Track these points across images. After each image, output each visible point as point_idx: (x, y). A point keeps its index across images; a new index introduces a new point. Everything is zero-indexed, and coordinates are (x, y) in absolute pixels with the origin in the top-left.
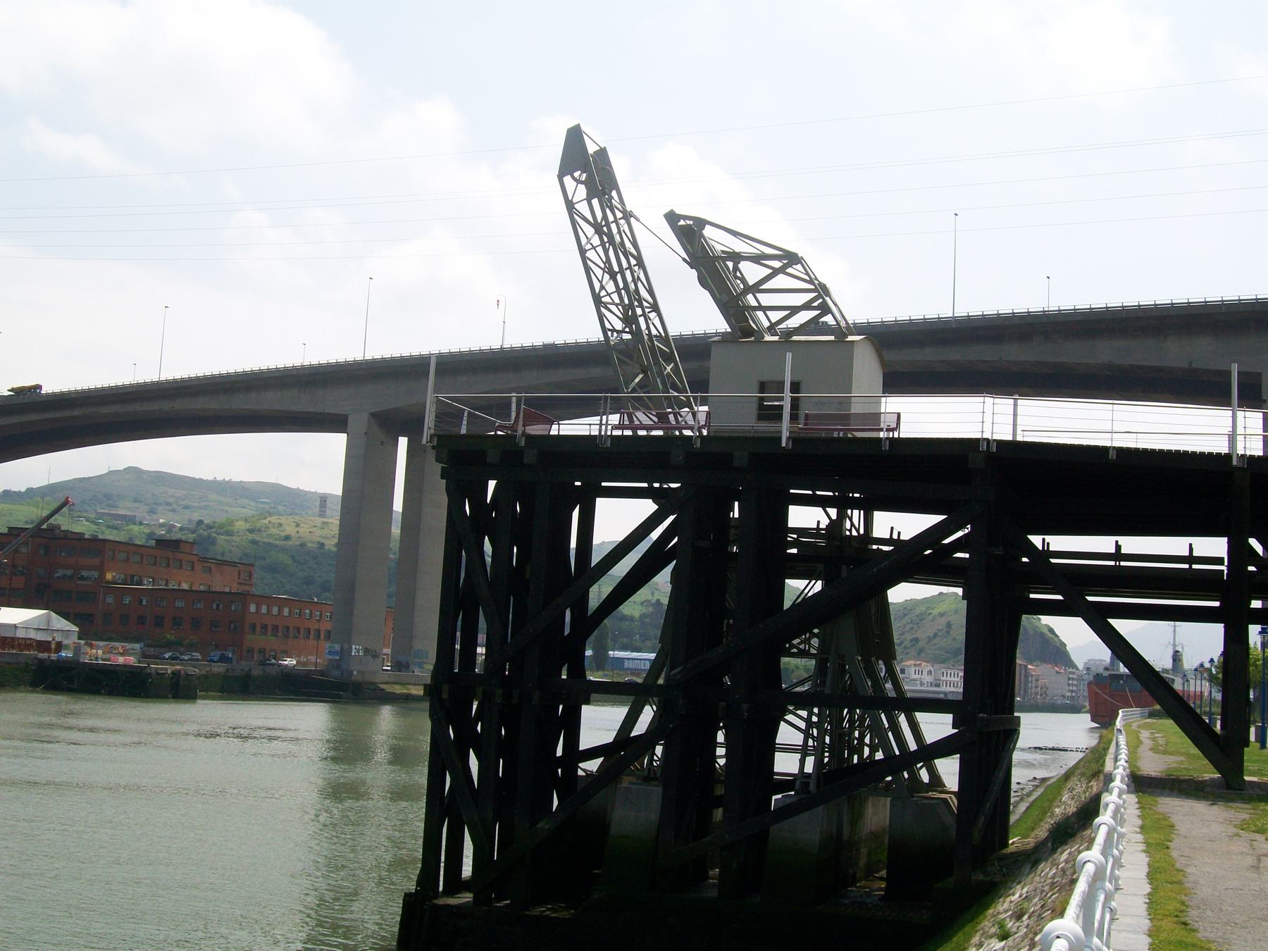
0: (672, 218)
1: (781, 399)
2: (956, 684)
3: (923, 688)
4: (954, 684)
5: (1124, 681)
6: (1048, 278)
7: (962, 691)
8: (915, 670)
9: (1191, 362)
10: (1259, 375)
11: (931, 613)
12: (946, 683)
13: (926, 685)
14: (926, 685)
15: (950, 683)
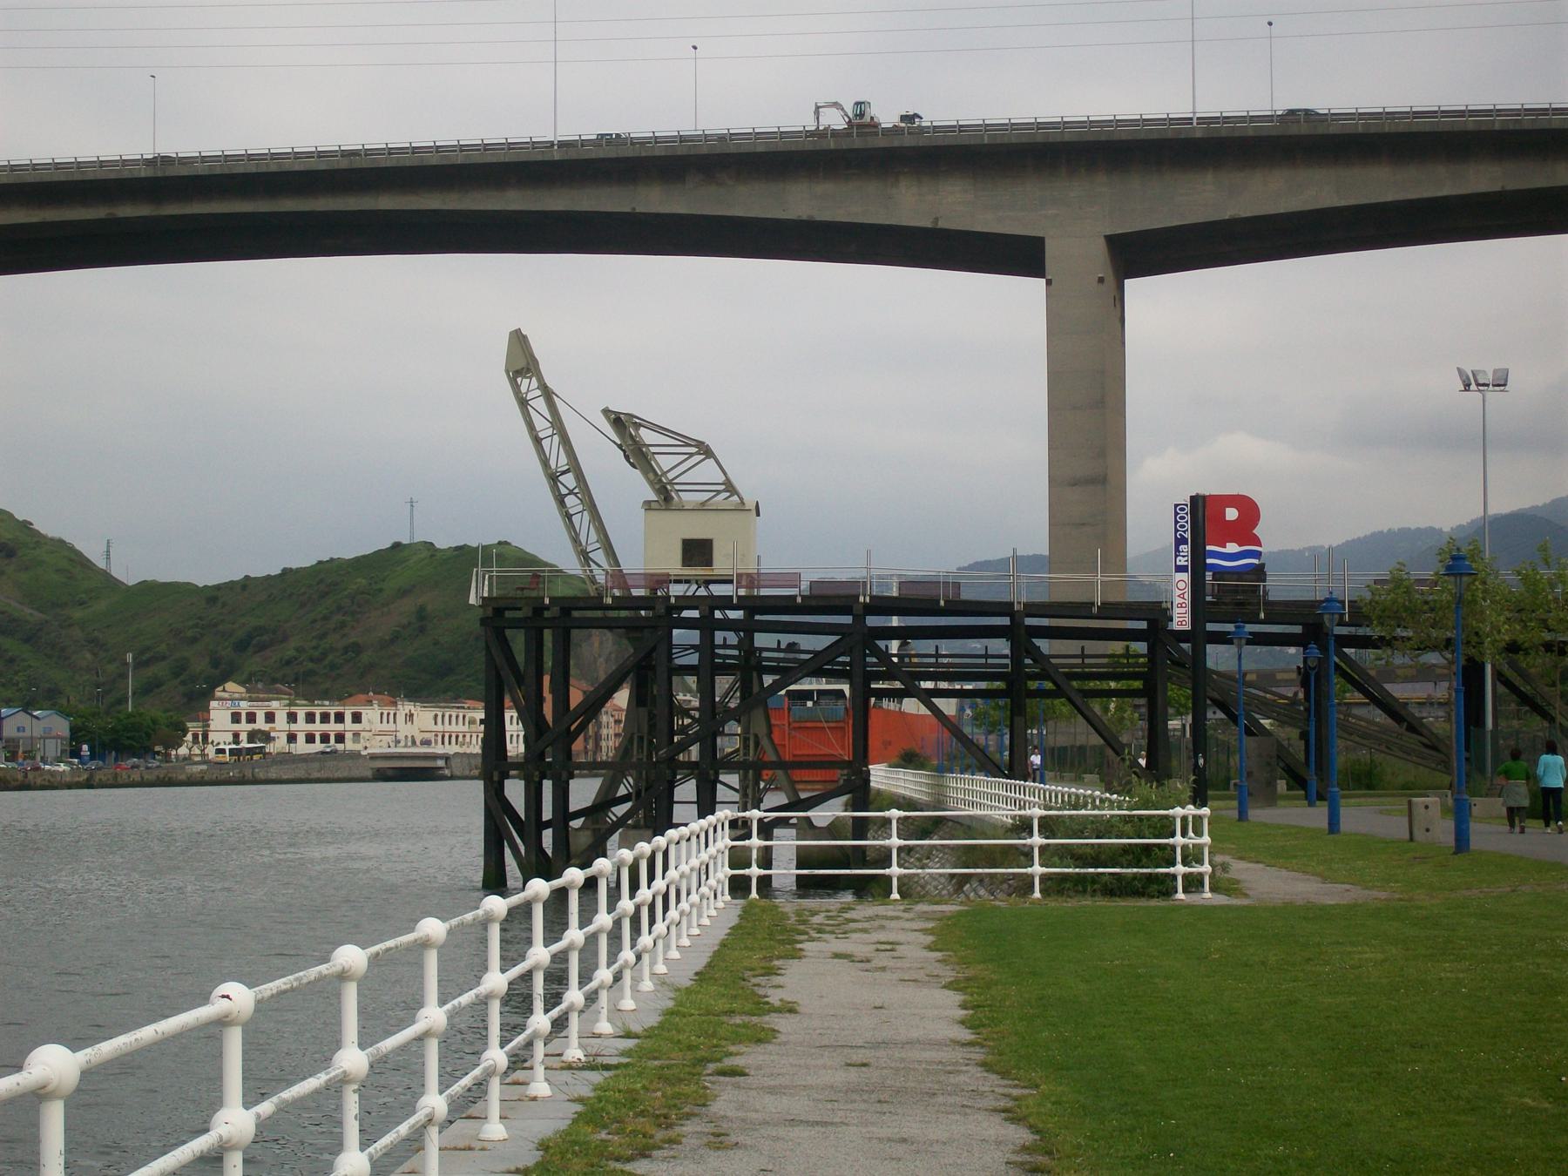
0: (606, 412)
1: (1184, 834)
2: (460, 739)
3: (399, 750)
4: (457, 737)
5: (815, 703)
6: (695, 48)
7: (480, 752)
8: (382, 714)
9: (937, 219)
10: (1040, 242)
11: (381, 590)
12: (443, 737)
13: (402, 743)
14: (402, 743)
15: (450, 737)
